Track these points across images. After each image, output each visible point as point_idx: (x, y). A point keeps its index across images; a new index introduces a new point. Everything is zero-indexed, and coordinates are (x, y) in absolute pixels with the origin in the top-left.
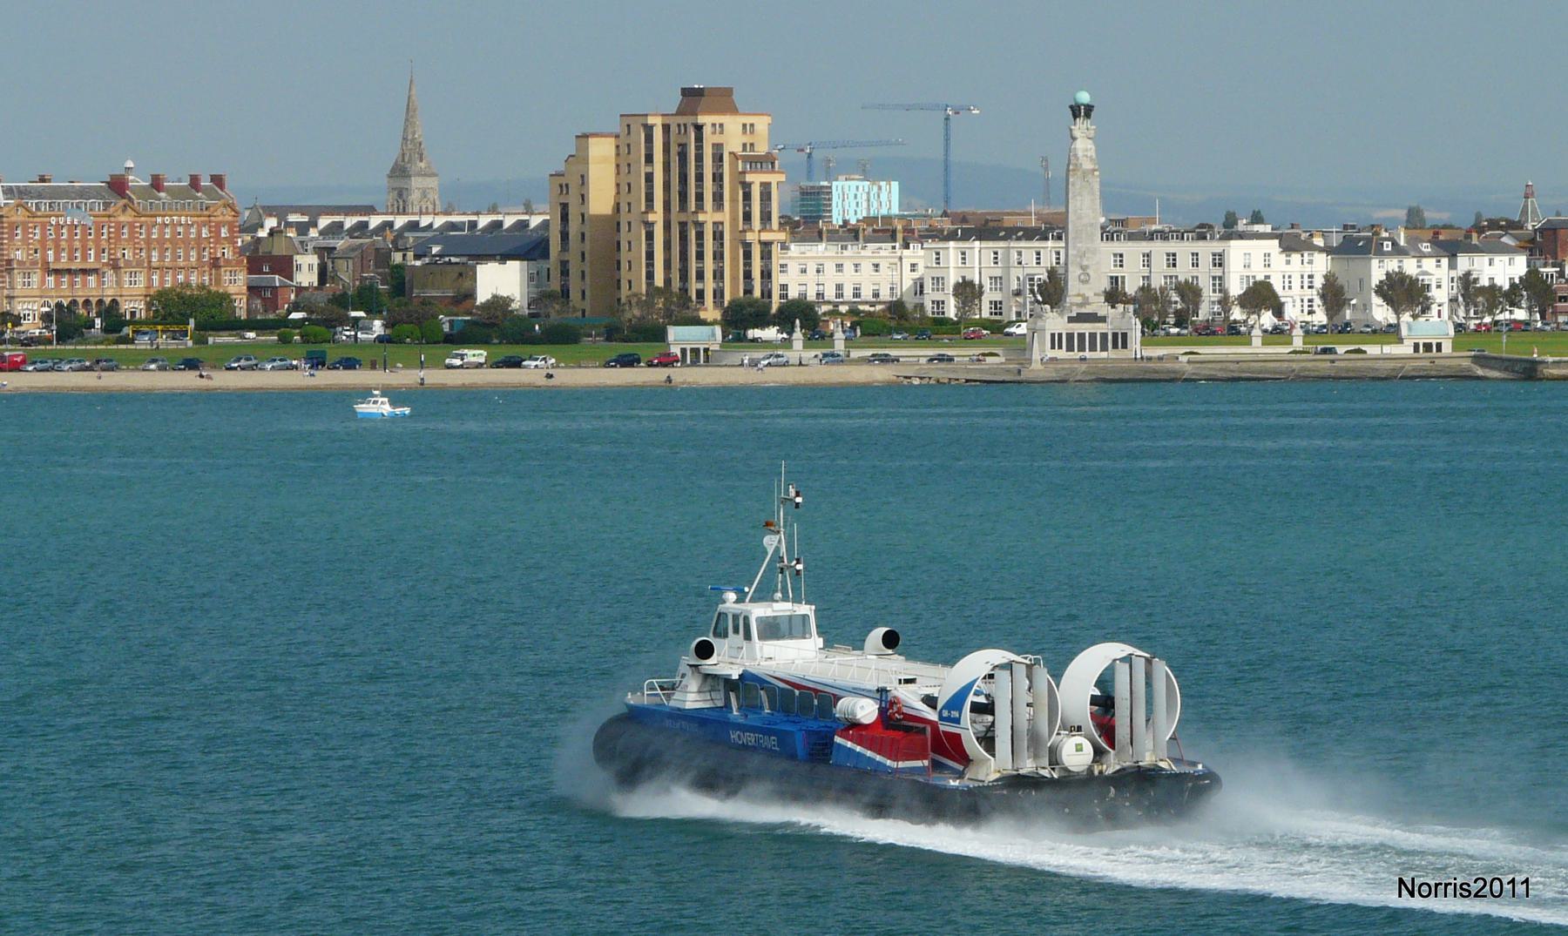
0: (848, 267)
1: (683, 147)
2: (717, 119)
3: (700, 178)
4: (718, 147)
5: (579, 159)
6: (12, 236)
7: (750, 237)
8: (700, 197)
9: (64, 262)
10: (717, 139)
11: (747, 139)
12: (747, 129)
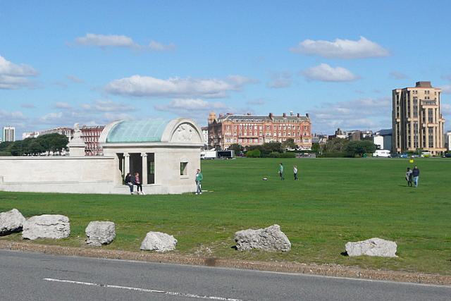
3: (409, 107)
6: (225, 129)
7: (424, 125)
9: (251, 136)
11: (427, 96)
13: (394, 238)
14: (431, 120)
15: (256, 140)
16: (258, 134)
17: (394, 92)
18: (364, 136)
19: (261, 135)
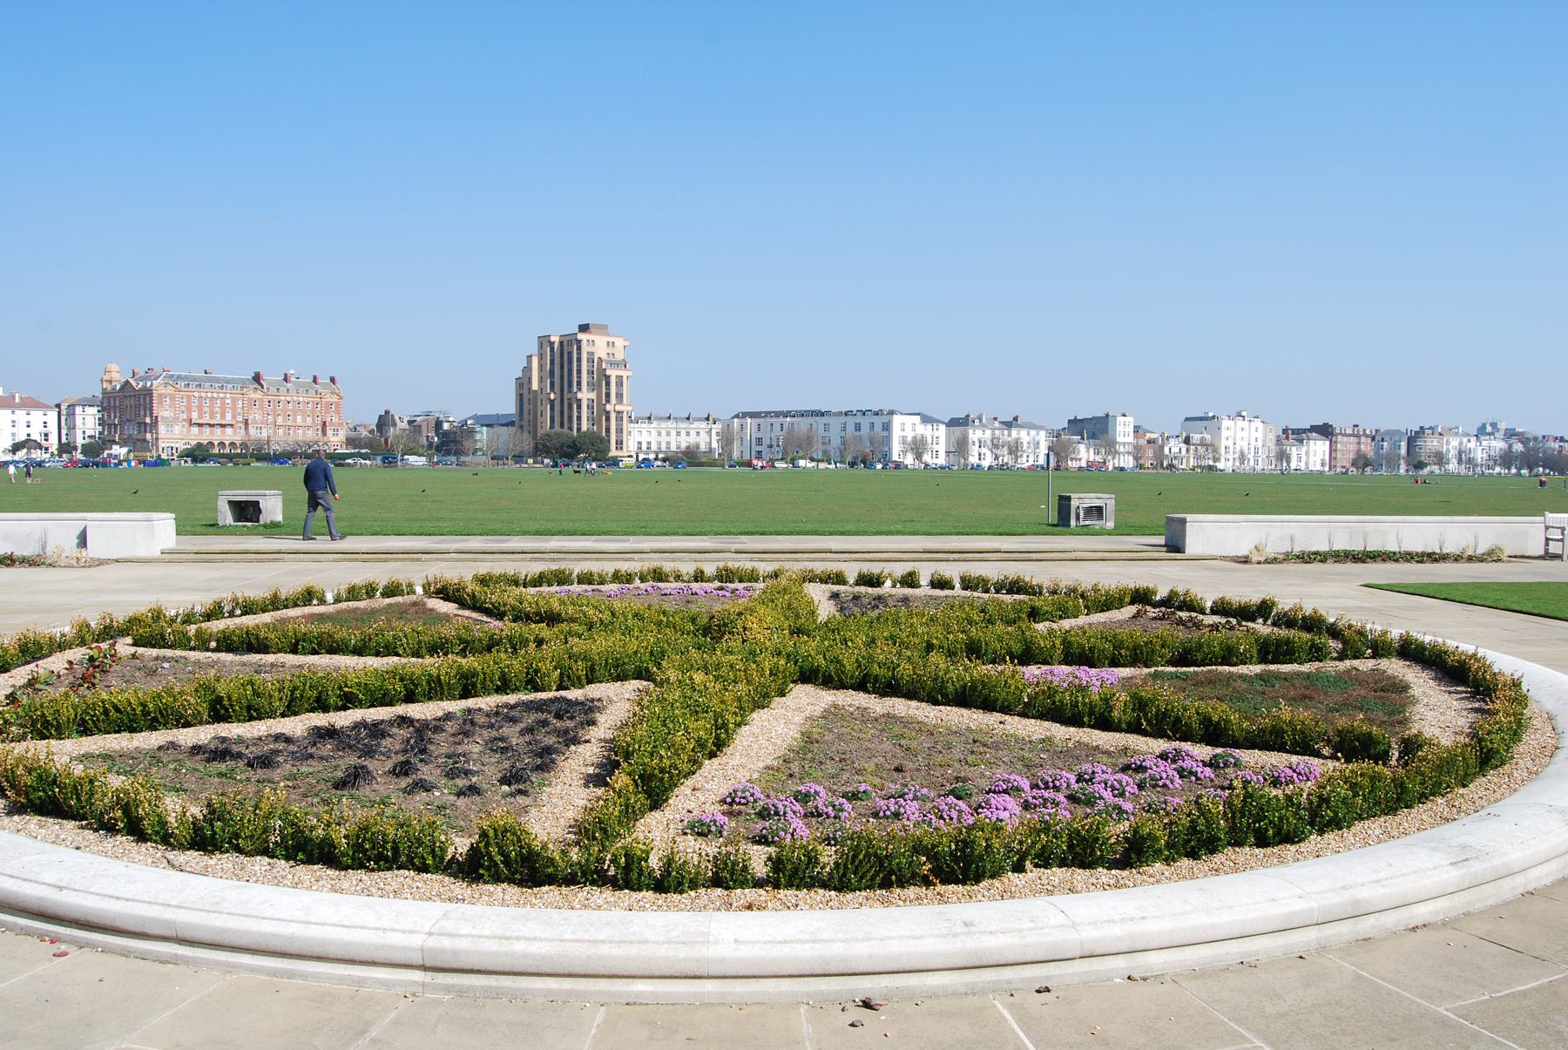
1: (570, 354)
3: (579, 372)
6: (160, 403)
7: (609, 407)
8: (579, 383)
10: (590, 349)
11: (610, 351)
12: (611, 344)
14: (620, 396)
15: (229, 430)
16: (234, 417)
17: (544, 341)
18: (446, 426)
19: (240, 418)
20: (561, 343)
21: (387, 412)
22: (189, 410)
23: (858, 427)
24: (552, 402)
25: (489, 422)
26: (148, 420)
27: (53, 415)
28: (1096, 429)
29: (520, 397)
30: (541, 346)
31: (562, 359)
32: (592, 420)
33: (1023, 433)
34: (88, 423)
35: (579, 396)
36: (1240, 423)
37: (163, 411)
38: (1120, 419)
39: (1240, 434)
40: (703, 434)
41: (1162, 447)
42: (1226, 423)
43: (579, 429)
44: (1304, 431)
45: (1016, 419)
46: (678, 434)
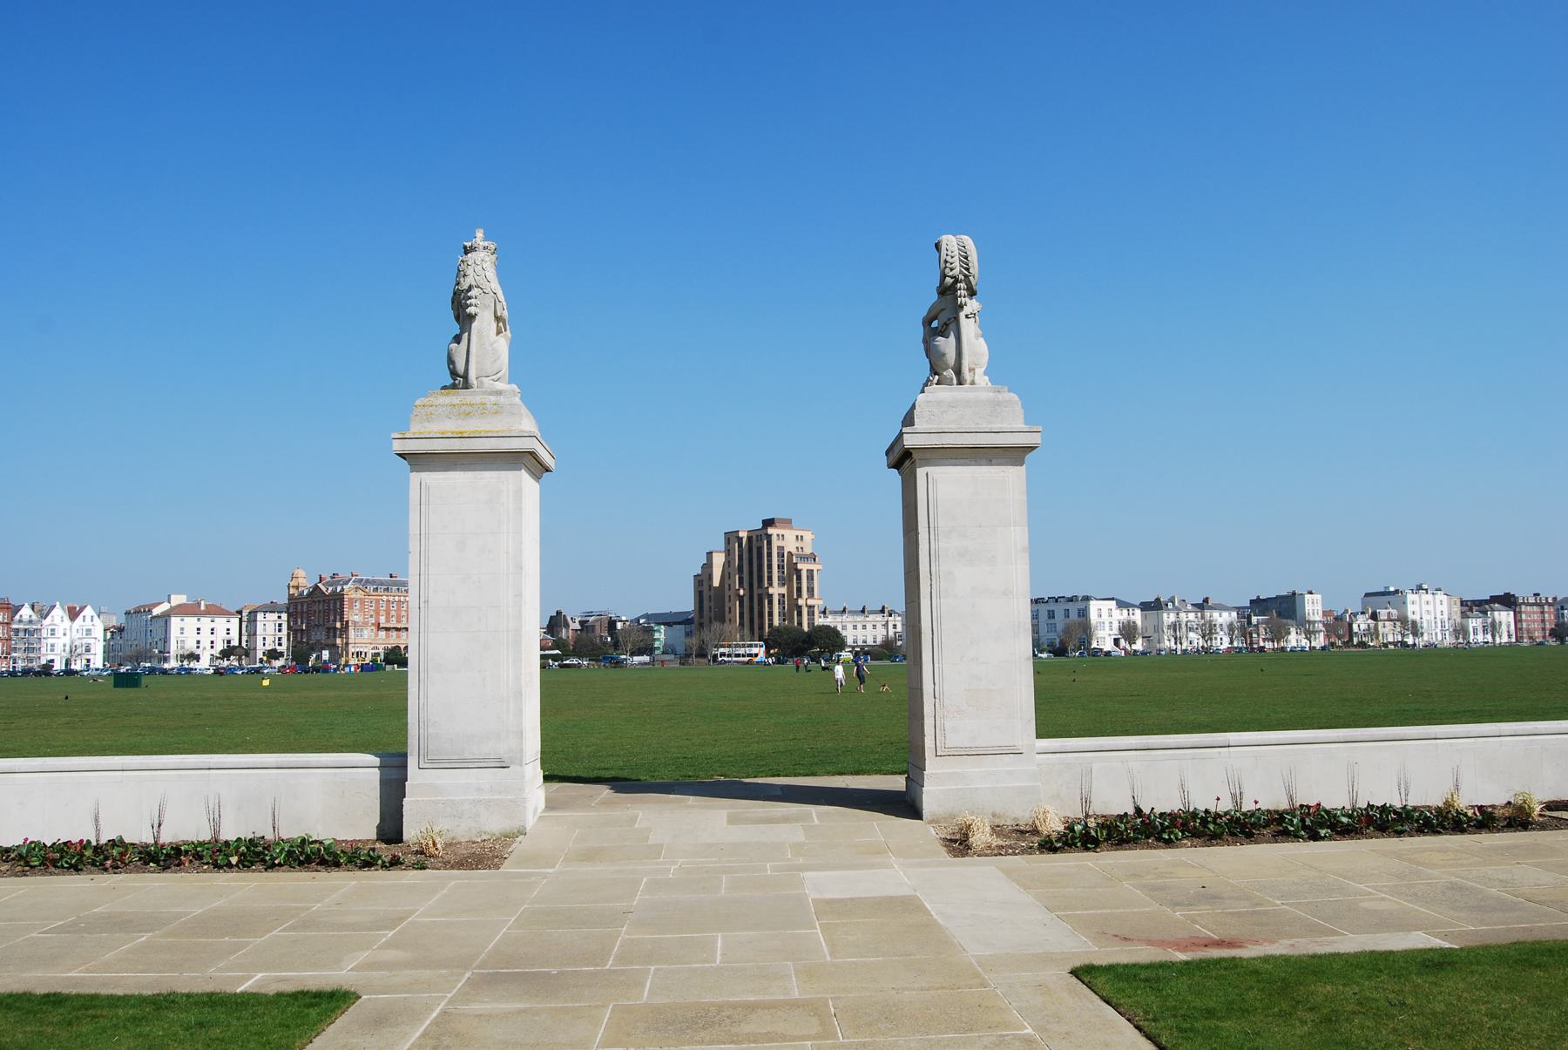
0: (869, 626)
1: (760, 550)
2: (781, 532)
3: (770, 566)
4: (781, 548)
5: (708, 567)
6: (351, 607)
7: (801, 602)
8: (770, 578)
10: (780, 543)
11: (799, 544)
12: (799, 538)
13: (1173, 823)
14: (811, 591)
17: (732, 537)
18: (619, 626)
20: (750, 539)
21: (559, 613)
22: (378, 614)
23: (1051, 615)
24: (741, 599)
25: (669, 621)
26: (338, 625)
27: (235, 621)
28: (1284, 609)
29: (699, 596)
30: (728, 541)
31: (751, 553)
32: (782, 614)
33: (1216, 614)
34: (271, 632)
35: (771, 591)
36: (1426, 597)
37: (353, 615)
38: (1307, 597)
39: (1425, 607)
40: (879, 626)
41: (1350, 625)
42: (1410, 597)
43: (771, 625)
44: (1486, 602)
45: (1206, 600)
46: (855, 627)
